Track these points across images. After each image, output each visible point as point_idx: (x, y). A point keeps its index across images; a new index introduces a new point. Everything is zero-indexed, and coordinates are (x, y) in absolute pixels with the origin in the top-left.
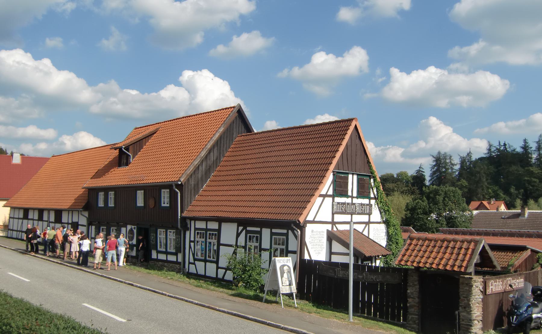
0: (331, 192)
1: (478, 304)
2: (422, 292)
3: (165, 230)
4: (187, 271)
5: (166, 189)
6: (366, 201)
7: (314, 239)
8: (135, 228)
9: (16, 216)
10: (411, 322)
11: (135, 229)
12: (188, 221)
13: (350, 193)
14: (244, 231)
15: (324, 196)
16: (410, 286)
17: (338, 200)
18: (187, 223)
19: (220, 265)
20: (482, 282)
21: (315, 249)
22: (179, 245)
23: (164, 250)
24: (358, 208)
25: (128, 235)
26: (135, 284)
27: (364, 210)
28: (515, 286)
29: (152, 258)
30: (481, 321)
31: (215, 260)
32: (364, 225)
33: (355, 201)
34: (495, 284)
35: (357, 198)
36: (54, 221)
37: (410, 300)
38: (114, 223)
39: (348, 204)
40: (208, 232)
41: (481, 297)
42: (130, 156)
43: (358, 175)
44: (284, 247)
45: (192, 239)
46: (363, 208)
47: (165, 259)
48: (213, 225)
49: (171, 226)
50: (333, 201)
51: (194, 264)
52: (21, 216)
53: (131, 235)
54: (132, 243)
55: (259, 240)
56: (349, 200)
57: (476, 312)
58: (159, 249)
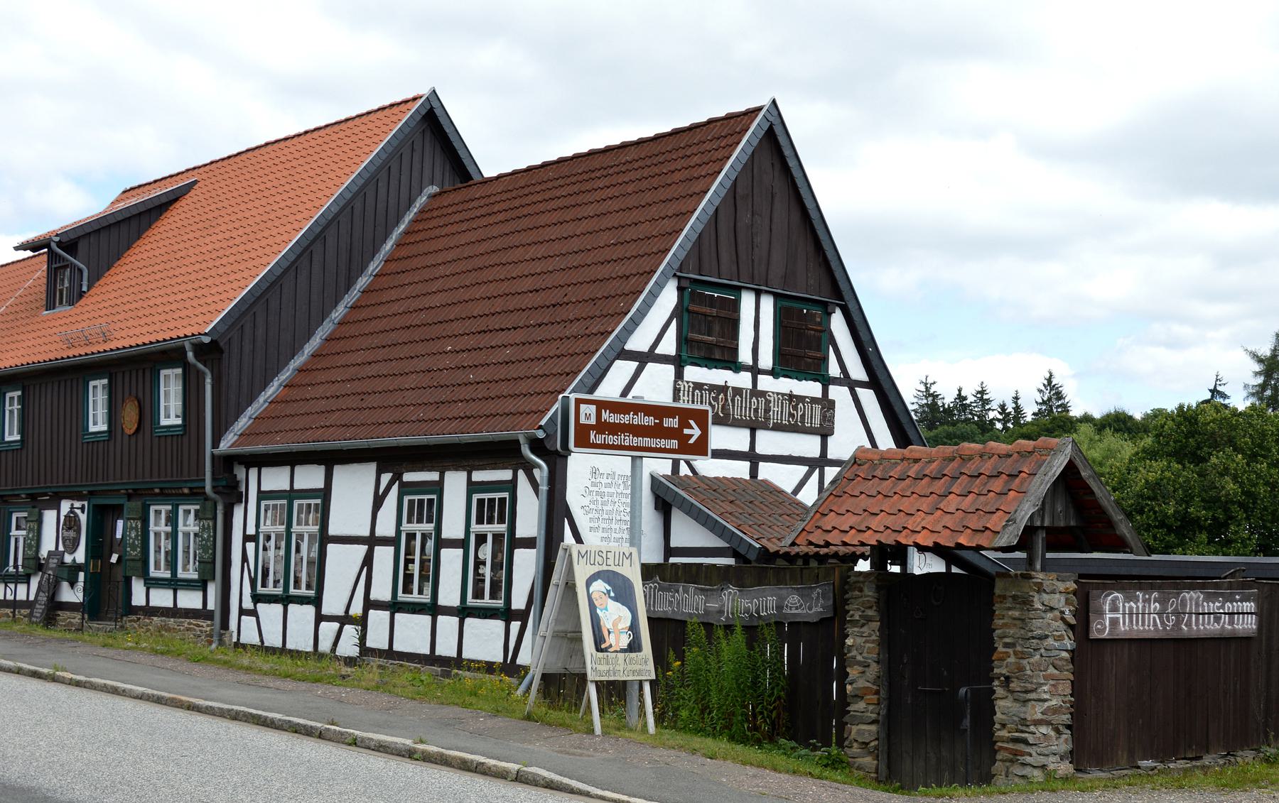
0: (669, 346)
1: (1056, 669)
2: (889, 642)
4: (235, 640)
5: (173, 368)
6: (812, 389)
7: (599, 498)
8: (82, 509)
10: (856, 749)
11: (83, 512)
12: (240, 472)
13: (745, 356)
15: (644, 359)
17: (694, 373)
20: (1074, 595)
21: (605, 535)
22: (210, 551)
23: (168, 575)
24: (776, 409)
25: (63, 534)
28: (1218, 624)
30: (1069, 727)
31: (312, 593)
32: (805, 469)
33: (765, 383)
34: (1127, 605)
35: (773, 373)
37: (853, 672)
39: (737, 391)
40: (296, 503)
41: (1069, 644)
42: (81, 271)
43: (776, 295)
44: (502, 528)
45: (251, 531)
46: (795, 408)
48: (310, 477)
49: (186, 491)
50: (679, 375)
51: (253, 613)
53: (72, 534)
54: (74, 560)
55: (434, 512)
56: (742, 380)
57: (1046, 696)
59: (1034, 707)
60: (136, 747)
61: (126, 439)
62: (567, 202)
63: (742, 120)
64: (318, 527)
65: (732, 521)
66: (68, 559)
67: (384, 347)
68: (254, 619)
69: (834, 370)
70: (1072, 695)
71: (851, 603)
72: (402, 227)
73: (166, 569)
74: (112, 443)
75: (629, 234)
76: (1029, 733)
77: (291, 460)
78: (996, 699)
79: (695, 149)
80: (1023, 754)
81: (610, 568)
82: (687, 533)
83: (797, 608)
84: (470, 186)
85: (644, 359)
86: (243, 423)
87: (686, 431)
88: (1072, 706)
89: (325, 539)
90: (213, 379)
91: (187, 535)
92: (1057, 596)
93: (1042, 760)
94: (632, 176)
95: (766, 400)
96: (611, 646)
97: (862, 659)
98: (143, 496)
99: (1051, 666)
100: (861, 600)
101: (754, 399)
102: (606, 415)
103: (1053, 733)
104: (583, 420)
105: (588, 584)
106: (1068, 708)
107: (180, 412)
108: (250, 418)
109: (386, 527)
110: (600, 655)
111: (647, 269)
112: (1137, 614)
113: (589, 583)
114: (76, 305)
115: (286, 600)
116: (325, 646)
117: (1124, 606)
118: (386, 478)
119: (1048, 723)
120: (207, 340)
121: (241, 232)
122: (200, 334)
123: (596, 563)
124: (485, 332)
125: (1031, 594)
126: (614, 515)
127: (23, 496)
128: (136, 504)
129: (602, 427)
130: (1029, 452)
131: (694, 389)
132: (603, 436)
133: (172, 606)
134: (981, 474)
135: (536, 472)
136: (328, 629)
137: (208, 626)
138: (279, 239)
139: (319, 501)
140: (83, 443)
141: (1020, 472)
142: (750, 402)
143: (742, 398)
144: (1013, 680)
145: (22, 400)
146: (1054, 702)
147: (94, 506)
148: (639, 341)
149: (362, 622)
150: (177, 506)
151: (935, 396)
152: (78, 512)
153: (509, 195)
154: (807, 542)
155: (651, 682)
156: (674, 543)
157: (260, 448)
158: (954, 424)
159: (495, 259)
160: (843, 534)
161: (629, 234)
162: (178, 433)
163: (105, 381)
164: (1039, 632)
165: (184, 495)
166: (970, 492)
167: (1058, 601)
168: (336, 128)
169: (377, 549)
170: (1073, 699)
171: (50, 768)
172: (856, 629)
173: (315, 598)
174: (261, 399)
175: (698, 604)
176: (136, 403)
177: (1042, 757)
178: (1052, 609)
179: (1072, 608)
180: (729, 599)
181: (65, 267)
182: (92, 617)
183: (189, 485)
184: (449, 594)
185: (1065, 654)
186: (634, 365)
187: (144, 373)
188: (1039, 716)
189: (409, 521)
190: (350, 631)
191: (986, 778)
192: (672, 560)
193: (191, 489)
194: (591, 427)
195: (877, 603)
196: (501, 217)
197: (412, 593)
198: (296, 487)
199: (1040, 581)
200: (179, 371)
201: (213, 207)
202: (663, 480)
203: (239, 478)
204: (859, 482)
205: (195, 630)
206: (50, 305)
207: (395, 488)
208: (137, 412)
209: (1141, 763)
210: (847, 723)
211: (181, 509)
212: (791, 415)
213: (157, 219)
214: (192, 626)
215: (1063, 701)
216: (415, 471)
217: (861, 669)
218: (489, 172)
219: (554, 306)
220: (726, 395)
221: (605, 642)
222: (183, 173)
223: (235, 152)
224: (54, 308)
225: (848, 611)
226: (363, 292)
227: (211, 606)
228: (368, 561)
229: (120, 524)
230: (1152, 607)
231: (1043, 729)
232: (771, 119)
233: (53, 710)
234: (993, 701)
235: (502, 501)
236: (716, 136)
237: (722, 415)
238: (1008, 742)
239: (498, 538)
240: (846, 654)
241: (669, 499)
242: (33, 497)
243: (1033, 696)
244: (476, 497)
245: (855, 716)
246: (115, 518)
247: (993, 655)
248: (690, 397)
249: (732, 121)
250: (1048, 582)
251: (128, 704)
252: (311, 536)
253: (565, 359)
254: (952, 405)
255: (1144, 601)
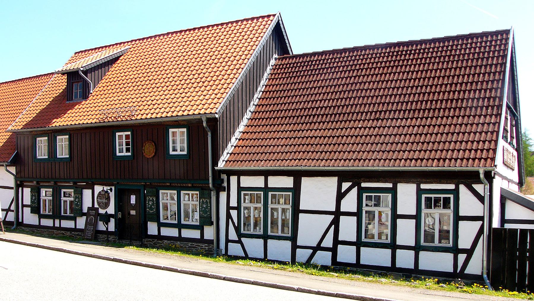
3: (176, 192)
11: (111, 191)
23: (176, 222)
25: (97, 200)
29: (149, 233)
38: (68, 182)
40: (270, 194)
49: (190, 185)
58: (162, 220)
66: (102, 211)
244: (424, 196)
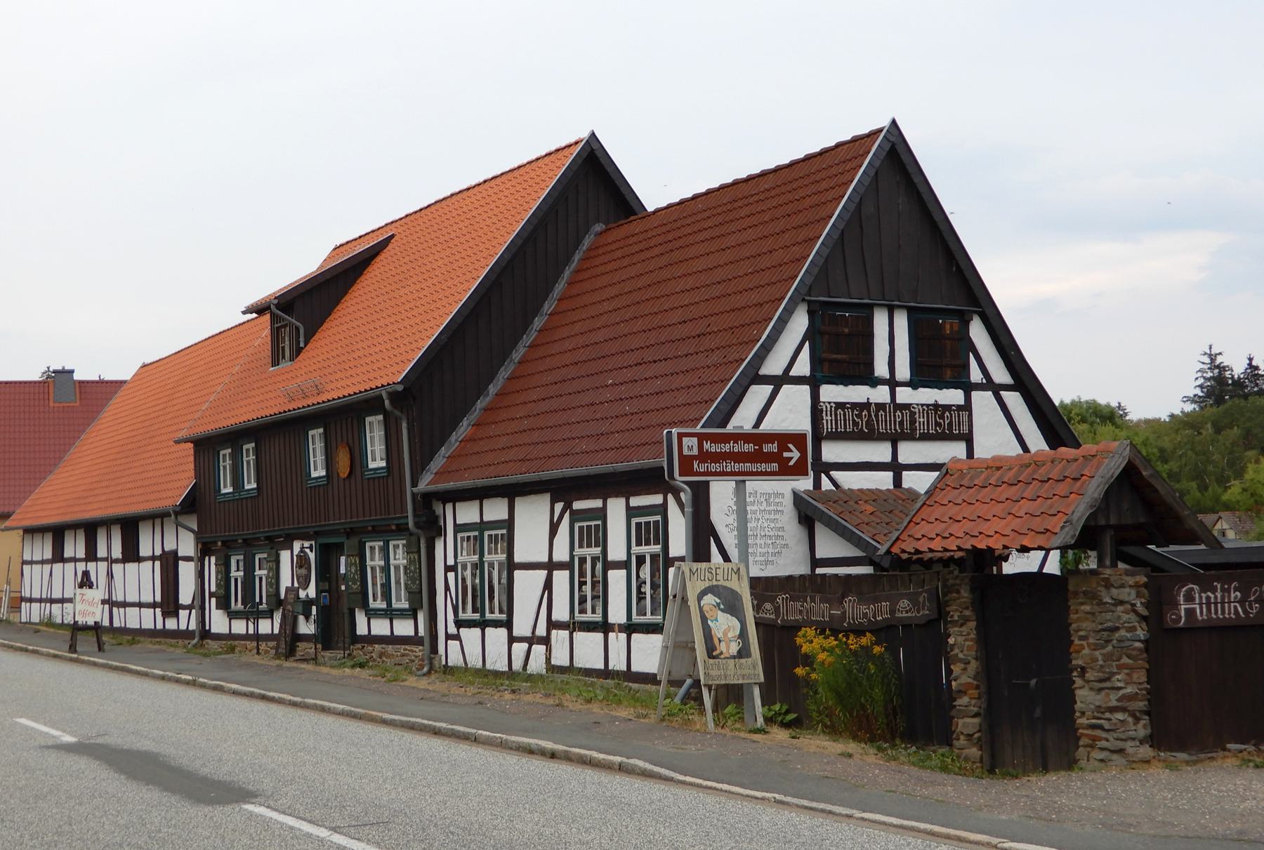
0: (803, 367)
2: (984, 638)
6: (954, 396)
8: (311, 548)
9: (37, 557)
11: (312, 551)
12: (438, 508)
13: (881, 369)
14: (567, 516)
16: (954, 623)
17: (831, 393)
18: (434, 511)
19: (516, 633)
22: (417, 582)
23: (384, 606)
24: (922, 420)
26: (513, 738)
27: (950, 424)
30: (1148, 713)
31: (504, 617)
33: (905, 395)
35: (913, 384)
36: (120, 556)
39: (880, 406)
40: (486, 534)
41: (1141, 634)
44: (657, 548)
45: (451, 562)
46: (942, 417)
47: (389, 633)
48: (496, 510)
49: (394, 527)
51: (457, 637)
52: (48, 555)
53: (303, 571)
54: (307, 595)
55: (600, 537)
57: (1119, 685)
59: (1108, 695)
60: (322, 751)
61: (341, 483)
62: (717, 232)
63: (866, 142)
64: (505, 556)
65: (868, 531)
67: (556, 383)
68: (458, 642)
69: (976, 375)
70: (1148, 683)
71: (950, 605)
72: (574, 265)
73: (382, 601)
74: (330, 486)
75: (766, 262)
76: (1104, 719)
77: (480, 494)
78: (1076, 688)
79: (823, 174)
80: (1100, 739)
81: (719, 583)
82: (829, 545)
83: (907, 612)
84: (631, 222)
85: (778, 382)
86: (437, 463)
87: (786, 455)
88: (1148, 693)
89: (511, 566)
90: (408, 424)
91: (397, 568)
92: (1127, 590)
93: (1120, 744)
94: (769, 204)
95: (911, 412)
96: (722, 653)
97: (963, 657)
98: (358, 534)
99: (1124, 656)
100: (959, 601)
101: (898, 413)
102: (707, 446)
103: (1130, 720)
104: (686, 452)
105: (700, 598)
106: (1144, 695)
107: (384, 456)
108: (444, 457)
109: (561, 554)
110: (711, 661)
111: (778, 296)
112: (1216, 603)
113: (700, 598)
114: (295, 361)
115: (483, 624)
116: (517, 665)
117: (1201, 598)
118: (559, 507)
119: (1124, 710)
120: (400, 388)
121: (429, 283)
122: (394, 383)
123: (706, 579)
124: (641, 364)
125: (1099, 589)
126: (758, 532)
127: (262, 538)
128: (354, 541)
129: (704, 456)
130: (1093, 456)
131: (836, 409)
132: (706, 465)
133: (389, 634)
134: (1049, 479)
135: (682, 495)
136: (518, 649)
137: (420, 651)
138: (460, 289)
139: (504, 531)
140: (307, 489)
141: (1082, 475)
142: (895, 416)
143: (885, 412)
144: (1088, 670)
145: (257, 451)
146: (1129, 690)
147: (320, 545)
148: (774, 365)
149: (546, 641)
150: (388, 541)
151: (1222, 368)
152: (308, 551)
153: (664, 229)
154: (900, 550)
155: (760, 685)
156: (819, 554)
157: (451, 485)
158: (1246, 397)
159: (650, 293)
160: (930, 541)
161: (766, 262)
162: (383, 474)
163: (321, 430)
164: (1110, 624)
165: (392, 531)
166: (1038, 497)
167: (1128, 594)
168: (510, 176)
169: (555, 573)
170: (1149, 686)
171: (251, 768)
172: (956, 629)
173: (507, 621)
174: (453, 438)
175: (823, 612)
176: (348, 449)
177: (1119, 742)
178: (1122, 603)
179: (1143, 600)
180: (849, 606)
181: (285, 326)
182: (326, 647)
183: (395, 522)
184: (617, 614)
185: (1138, 645)
186: (769, 388)
187: (352, 420)
188: (1114, 703)
189: (581, 546)
190: (539, 649)
191: (1070, 764)
192: (819, 571)
193: (373, 527)
194: (693, 458)
195: (973, 603)
196: (657, 251)
197: (586, 613)
198: (486, 519)
199: (1107, 576)
200: (381, 417)
201: (406, 260)
202: (804, 495)
203: (437, 513)
204: (949, 490)
205: (410, 655)
206: (275, 362)
207: (567, 515)
208: (349, 456)
209: (1229, 746)
210: (953, 718)
211: (391, 544)
212: (938, 424)
213: (361, 274)
214: (407, 652)
215: (1139, 690)
216: (582, 499)
217: (962, 666)
218: (650, 208)
219: (699, 336)
220: (869, 412)
221: (716, 650)
222: (383, 227)
223: (426, 205)
224: (278, 365)
225: (949, 612)
226: (540, 331)
227: (422, 632)
228: (548, 585)
229: (343, 559)
230: (1233, 595)
231: (1120, 716)
232: (892, 139)
233: (269, 725)
234: (1073, 691)
235: (656, 523)
236: (842, 160)
237: (866, 431)
238: (1087, 729)
239: (654, 557)
240: (949, 653)
241: (810, 513)
242: (270, 539)
243: (1107, 684)
244: (634, 521)
245: (960, 710)
246: (339, 555)
247: (1070, 647)
248: (833, 416)
249: (857, 143)
250: (1116, 578)
251: (330, 719)
252: (500, 564)
253: (706, 387)
254: (1242, 376)
255: (1223, 590)
